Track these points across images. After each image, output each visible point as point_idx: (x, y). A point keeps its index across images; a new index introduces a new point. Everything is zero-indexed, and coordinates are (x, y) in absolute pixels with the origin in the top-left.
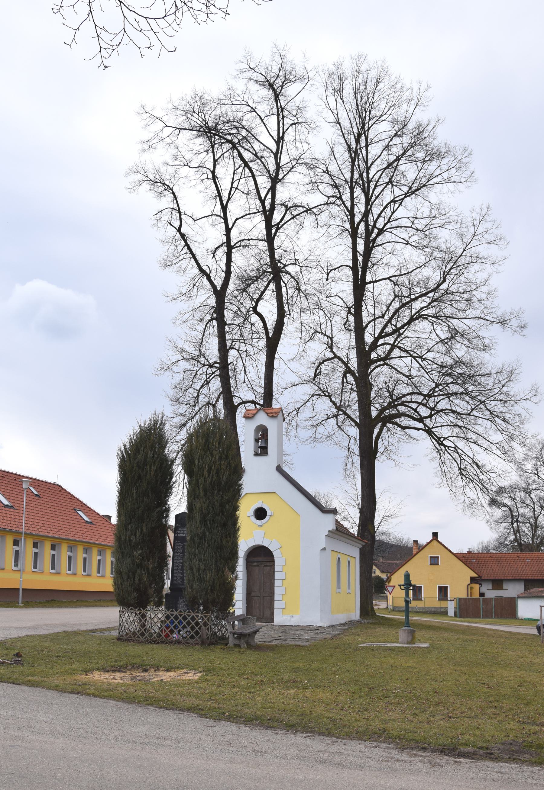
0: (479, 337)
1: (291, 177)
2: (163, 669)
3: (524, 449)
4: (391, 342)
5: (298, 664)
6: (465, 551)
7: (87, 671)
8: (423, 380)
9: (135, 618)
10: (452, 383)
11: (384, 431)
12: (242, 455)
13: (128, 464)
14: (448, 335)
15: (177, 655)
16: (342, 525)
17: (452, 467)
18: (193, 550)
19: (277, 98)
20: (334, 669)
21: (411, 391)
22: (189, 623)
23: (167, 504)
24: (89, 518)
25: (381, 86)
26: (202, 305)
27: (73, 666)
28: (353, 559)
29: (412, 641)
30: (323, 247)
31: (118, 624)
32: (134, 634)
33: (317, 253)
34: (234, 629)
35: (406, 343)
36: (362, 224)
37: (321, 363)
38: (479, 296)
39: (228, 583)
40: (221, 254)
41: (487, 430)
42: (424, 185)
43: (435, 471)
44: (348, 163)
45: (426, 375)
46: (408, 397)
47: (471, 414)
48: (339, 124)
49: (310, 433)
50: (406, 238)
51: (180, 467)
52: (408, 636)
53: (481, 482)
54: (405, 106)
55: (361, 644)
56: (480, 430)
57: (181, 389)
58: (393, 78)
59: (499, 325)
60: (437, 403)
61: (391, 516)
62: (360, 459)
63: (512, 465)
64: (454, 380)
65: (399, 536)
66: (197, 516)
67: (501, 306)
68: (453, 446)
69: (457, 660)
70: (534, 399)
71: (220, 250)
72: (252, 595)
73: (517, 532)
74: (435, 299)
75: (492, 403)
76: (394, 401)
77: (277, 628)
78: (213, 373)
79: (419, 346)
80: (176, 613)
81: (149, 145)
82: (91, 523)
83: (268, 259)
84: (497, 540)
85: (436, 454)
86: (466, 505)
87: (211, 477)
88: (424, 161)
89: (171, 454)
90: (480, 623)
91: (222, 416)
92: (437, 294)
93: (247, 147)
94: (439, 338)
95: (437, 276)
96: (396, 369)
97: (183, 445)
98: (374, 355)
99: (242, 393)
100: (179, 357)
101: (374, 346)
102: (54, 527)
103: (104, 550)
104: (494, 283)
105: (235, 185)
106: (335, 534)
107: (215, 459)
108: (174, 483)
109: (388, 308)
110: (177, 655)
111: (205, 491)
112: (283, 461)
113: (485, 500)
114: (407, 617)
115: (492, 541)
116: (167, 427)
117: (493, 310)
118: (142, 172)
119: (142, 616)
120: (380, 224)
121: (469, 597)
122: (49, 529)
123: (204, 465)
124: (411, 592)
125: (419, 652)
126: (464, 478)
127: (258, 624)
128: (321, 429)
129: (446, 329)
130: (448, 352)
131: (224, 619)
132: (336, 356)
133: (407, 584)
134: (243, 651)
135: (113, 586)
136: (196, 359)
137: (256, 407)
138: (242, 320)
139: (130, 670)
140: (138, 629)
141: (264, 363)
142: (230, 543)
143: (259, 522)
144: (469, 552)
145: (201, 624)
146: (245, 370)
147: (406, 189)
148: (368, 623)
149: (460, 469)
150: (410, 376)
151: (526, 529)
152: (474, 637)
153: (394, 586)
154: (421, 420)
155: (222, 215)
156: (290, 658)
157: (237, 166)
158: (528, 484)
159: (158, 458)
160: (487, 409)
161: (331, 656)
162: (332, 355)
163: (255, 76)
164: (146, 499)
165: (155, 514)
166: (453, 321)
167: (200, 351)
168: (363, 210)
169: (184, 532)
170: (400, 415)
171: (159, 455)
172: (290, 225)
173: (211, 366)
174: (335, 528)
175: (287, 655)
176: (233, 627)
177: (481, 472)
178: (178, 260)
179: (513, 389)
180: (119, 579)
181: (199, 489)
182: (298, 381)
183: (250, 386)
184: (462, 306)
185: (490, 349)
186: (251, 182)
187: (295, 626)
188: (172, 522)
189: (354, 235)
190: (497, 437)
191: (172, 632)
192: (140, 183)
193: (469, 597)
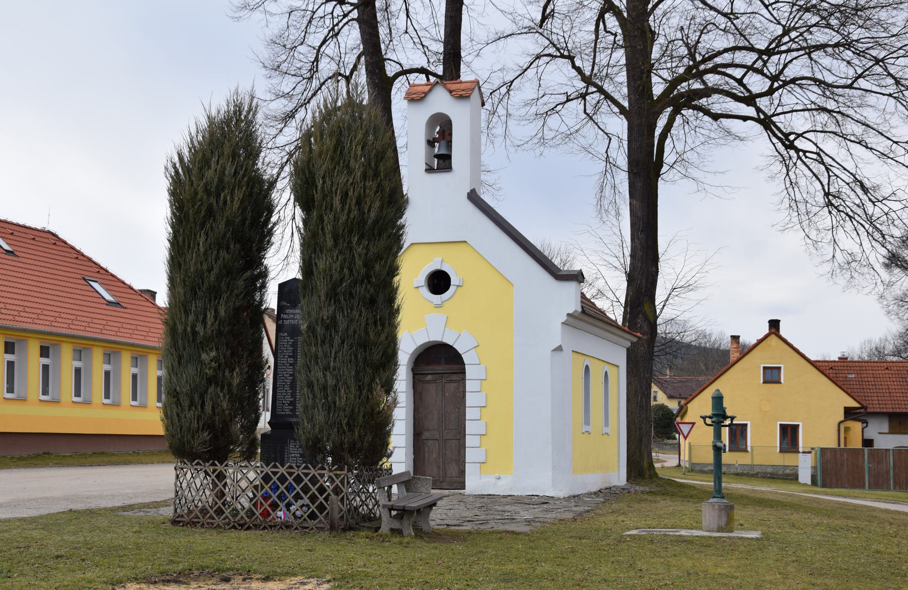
2: (258, 576)
5: (510, 567)
6: (834, 357)
8: (757, 21)
9: (205, 481)
10: (816, 25)
11: (675, 124)
12: (404, 171)
13: (187, 188)
15: (284, 551)
16: (593, 303)
17: (812, 190)
18: (313, 349)
20: (578, 576)
21: (732, 45)
22: (306, 490)
23: (262, 264)
24: (112, 296)
27: (89, 575)
28: (615, 369)
29: (728, 526)
31: (173, 495)
32: (204, 511)
34: (390, 500)
39: (379, 412)
41: (888, 117)
43: (777, 199)
45: (764, 12)
46: (726, 55)
47: (855, 85)
49: (533, 128)
52: (720, 517)
53: (870, 220)
55: (629, 529)
56: (871, 116)
57: (284, 46)
60: (785, 66)
61: (688, 287)
62: (629, 178)
64: (823, 18)
65: (701, 326)
66: (323, 288)
68: (814, 149)
69: (817, 565)
72: (423, 437)
76: (697, 65)
77: (471, 499)
78: (345, 16)
80: (282, 470)
82: (117, 304)
85: (778, 167)
86: (836, 264)
87: (346, 211)
89: (269, 171)
90: (865, 498)
99: (402, 53)
102: (45, 312)
103: (144, 357)
106: (580, 319)
108: (275, 224)
110: (284, 551)
111: (336, 238)
113: (878, 255)
115: (890, 338)
116: (260, 118)
119: (218, 477)
121: (842, 446)
122: (35, 316)
123: (334, 189)
124: (725, 432)
125: (742, 548)
126: (834, 212)
127: (436, 492)
128: (553, 121)
133: (719, 416)
134: (408, 543)
135: (162, 420)
137: (428, 79)
140: (210, 500)
142: (383, 337)
144: (843, 359)
145: (329, 491)
146: (407, 10)
148: (643, 492)
149: (827, 194)
150: (732, 13)
152: (850, 523)
153: (693, 424)
154: (750, 100)
156: (496, 556)
159: (244, 176)
160: (890, 74)
161: (573, 551)
164: (223, 253)
165: (241, 283)
170: (708, 92)
171: (246, 170)
174: (580, 310)
175: (490, 551)
176: (389, 495)
177: (870, 200)
180: (174, 406)
181: (324, 234)
182: (509, 28)
183: (417, 40)
187: (504, 497)
188: (271, 300)
191: (274, 506)
193: (842, 446)
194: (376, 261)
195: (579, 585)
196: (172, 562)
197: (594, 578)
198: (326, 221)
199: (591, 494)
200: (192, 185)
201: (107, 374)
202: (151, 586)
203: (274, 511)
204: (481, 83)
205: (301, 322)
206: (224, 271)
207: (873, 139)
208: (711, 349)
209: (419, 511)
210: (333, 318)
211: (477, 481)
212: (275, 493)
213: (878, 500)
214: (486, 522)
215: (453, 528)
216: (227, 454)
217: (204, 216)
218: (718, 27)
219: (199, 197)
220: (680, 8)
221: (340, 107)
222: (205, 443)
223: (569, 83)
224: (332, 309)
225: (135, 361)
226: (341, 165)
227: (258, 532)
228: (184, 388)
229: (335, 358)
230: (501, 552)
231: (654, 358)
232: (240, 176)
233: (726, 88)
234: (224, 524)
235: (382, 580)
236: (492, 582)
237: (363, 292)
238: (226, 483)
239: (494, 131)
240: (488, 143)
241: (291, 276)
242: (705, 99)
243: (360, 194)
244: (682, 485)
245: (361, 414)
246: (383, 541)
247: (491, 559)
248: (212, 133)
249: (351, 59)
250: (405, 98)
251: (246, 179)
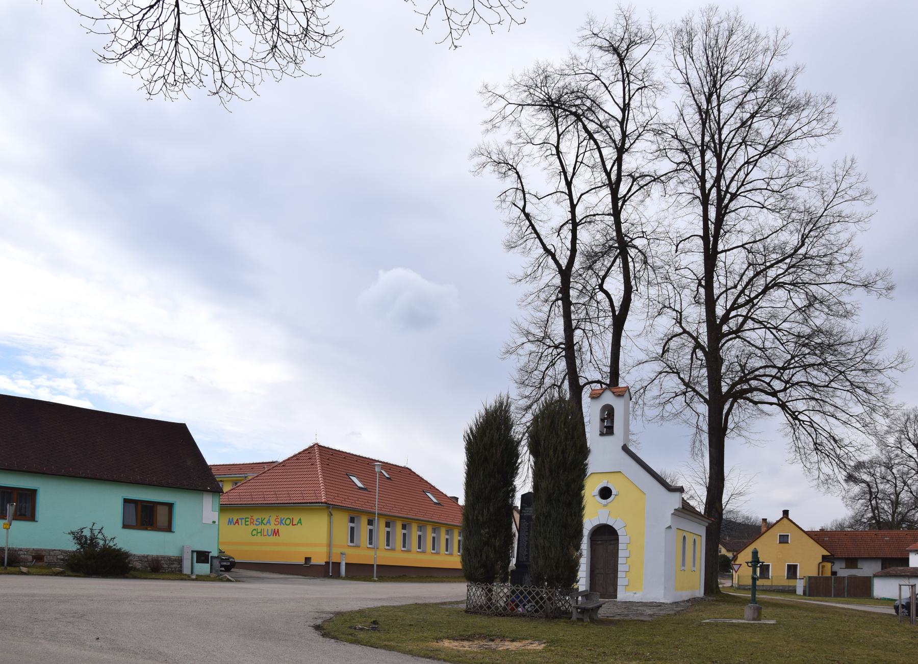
0: (840, 303)
1: (638, 146)
3: (887, 420)
4: (744, 314)
5: (640, 638)
6: (818, 529)
7: (438, 639)
10: (809, 354)
12: (588, 435)
14: (806, 303)
17: (807, 441)
19: (622, 63)
25: (734, 38)
26: (547, 285)
27: (425, 634)
29: (758, 618)
30: (671, 217)
32: (481, 607)
33: (666, 223)
35: (759, 314)
36: (714, 190)
37: (669, 340)
38: (840, 259)
40: (566, 233)
42: (782, 142)
43: (789, 446)
44: (698, 126)
45: (781, 347)
48: (689, 84)
49: (657, 411)
50: (762, 201)
51: (526, 448)
53: (838, 457)
54: (760, 57)
56: (839, 402)
58: (747, 28)
59: (862, 288)
61: (740, 494)
63: (873, 438)
65: (747, 514)
67: (865, 268)
70: (900, 367)
71: (565, 227)
73: (875, 508)
74: (793, 264)
75: (854, 373)
76: (746, 375)
79: (774, 316)
80: (521, 588)
81: (492, 125)
83: (615, 234)
84: (853, 517)
85: (789, 429)
88: (780, 116)
91: (568, 396)
92: (795, 259)
93: (591, 118)
94: (796, 306)
95: (795, 240)
96: (749, 342)
97: (528, 427)
98: (725, 328)
99: (588, 373)
100: (525, 340)
101: (726, 318)
104: (857, 243)
105: (580, 159)
107: (561, 438)
109: (741, 278)
112: (629, 440)
113: (841, 476)
114: (754, 594)
116: (512, 408)
117: (856, 273)
118: (486, 154)
120: (733, 189)
128: (668, 407)
129: (803, 296)
130: (805, 321)
131: (568, 595)
132: (685, 331)
133: (755, 560)
136: (541, 341)
138: (587, 299)
139: (478, 639)
141: (611, 341)
143: (604, 502)
144: (822, 530)
147: (761, 148)
149: (815, 444)
151: (886, 506)
154: (774, 394)
155: (567, 191)
157: (581, 139)
158: (890, 459)
162: (681, 330)
163: (599, 42)
166: (812, 287)
167: (545, 332)
168: (715, 174)
169: (530, 511)
170: (751, 390)
172: (637, 197)
173: (556, 347)
178: (522, 241)
179: (876, 357)
182: (645, 358)
184: (822, 270)
185: (853, 314)
186: (597, 155)
188: (518, 503)
189: (705, 203)
190: (858, 409)
191: (517, 606)
192: (484, 165)
201: (434, 538)
207: (839, 414)
209: (592, 609)
211: (623, 595)
213: (839, 603)
214: (627, 615)
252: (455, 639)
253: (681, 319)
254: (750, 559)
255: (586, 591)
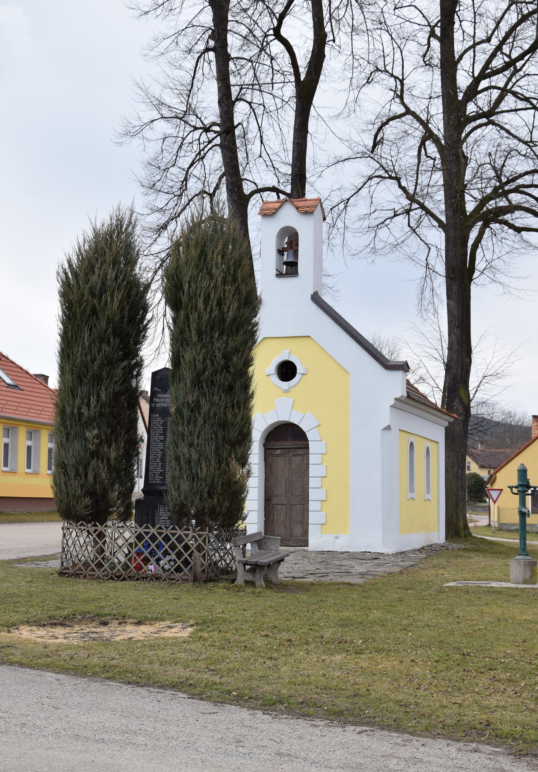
2: (132, 621)
5: (346, 614)
7: (10, 626)
9: (88, 540)
11: (485, 236)
12: (258, 276)
13: (75, 290)
15: (154, 599)
16: (416, 389)
18: (180, 428)
20: (405, 622)
21: (532, 168)
22: (173, 547)
23: (138, 355)
24: (12, 379)
28: (435, 444)
32: (86, 564)
34: (244, 557)
39: (235, 482)
46: (526, 177)
51: (159, 295)
52: (525, 571)
55: (448, 581)
57: (159, 168)
61: (496, 375)
62: (447, 282)
65: (509, 408)
66: (188, 375)
72: (273, 502)
77: (313, 555)
78: (210, 142)
80: (153, 531)
87: (208, 311)
89: (145, 275)
96: (508, 132)
97: (163, 261)
100: (155, 115)
101: (472, 92)
106: (406, 403)
108: (149, 321)
109: (497, 27)
110: (154, 599)
111: (200, 334)
114: (523, 539)
116: (138, 230)
119: (98, 536)
123: (198, 292)
128: (383, 233)
132: (408, 111)
134: (260, 593)
135: (52, 488)
136: (182, 118)
137: (279, 197)
139: (80, 622)
140: (92, 557)
142: (239, 418)
143: (285, 385)
145: (193, 548)
146: (261, 137)
148: (459, 549)
150: (531, 141)
153: (501, 490)
156: (335, 604)
159: (123, 280)
161: (400, 600)
162: (402, 110)
164: (105, 347)
165: (119, 371)
169: (166, 400)
170: (512, 208)
171: (125, 275)
173: (207, 130)
174: (405, 395)
175: (329, 599)
176: (244, 552)
180: (62, 476)
181: (190, 331)
183: (269, 163)
187: (342, 553)
188: (146, 384)
191: (146, 561)
194: (234, 354)
195: (405, 630)
196: (58, 608)
197: (418, 624)
198: (191, 320)
199: (415, 550)
200: (79, 288)
202: (41, 628)
203: (145, 565)
204: (323, 200)
205: (170, 405)
206: (106, 362)
208: (516, 426)
209: (269, 566)
210: (197, 403)
211: (317, 540)
212: (147, 550)
214: (326, 575)
215: (298, 580)
216: (107, 517)
217: (90, 315)
218: (519, 153)
219: (85, 298)
220: (488, 137)
221: (204, 220)
222: (87, 507)
223: (396, 201)
224: (196, 394)
225: (30, 435)
226: (205, 271)
227: (133, 583)
228: (71, 461)
229: (199, 436)
230: (339, 601)
231: (468, 435)
232: (120, 281)
233: (526, 205)
234: (103, 575)
235: (237, 625)
236: (331, 627)
237: (222, 380)
238: (105, 541)
239: (333, 241)
240: (329, 251)
241: (161, 366)
242: (509, 215)
243: (220, 297)
244: (491, 543)
245: (220, 483)
246: (238, 591)
247: (331, 607)
248: (96, 243)
249: (213, 179)
250: (259, 214)
251: (125, 283)
252: (40, 624)
253: (402, 91)
254: (515, 483)
255: (259, 534)
